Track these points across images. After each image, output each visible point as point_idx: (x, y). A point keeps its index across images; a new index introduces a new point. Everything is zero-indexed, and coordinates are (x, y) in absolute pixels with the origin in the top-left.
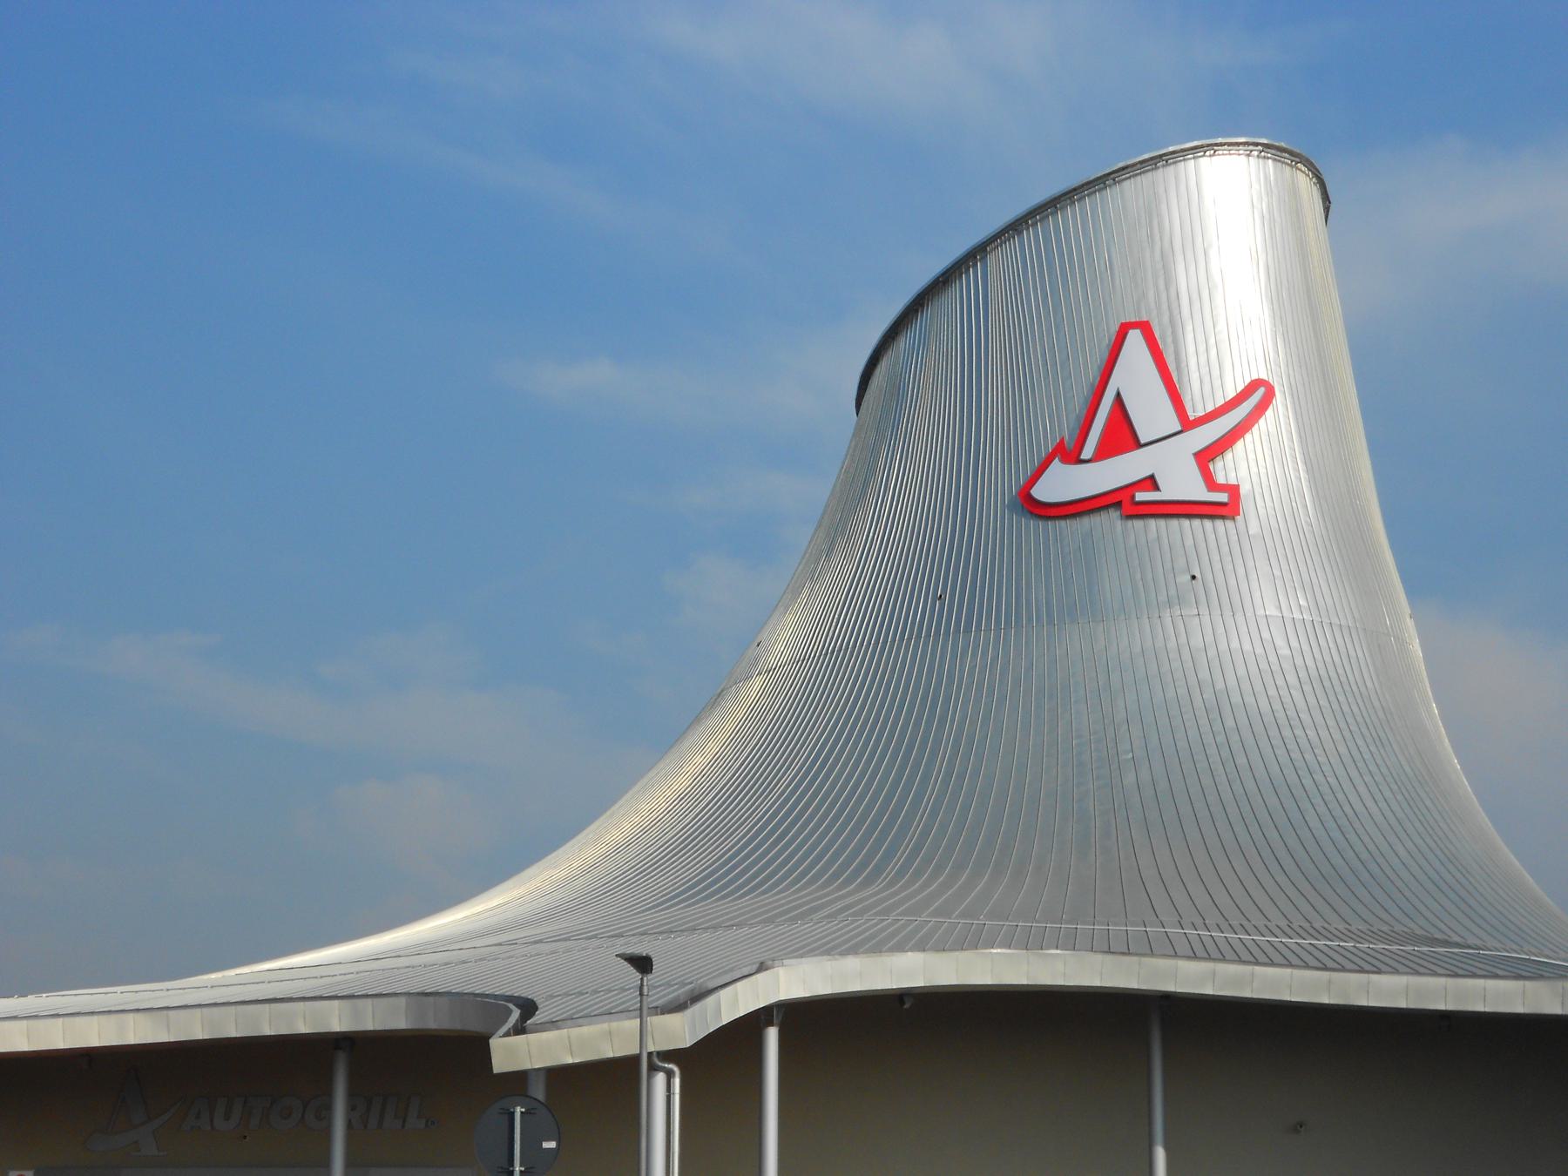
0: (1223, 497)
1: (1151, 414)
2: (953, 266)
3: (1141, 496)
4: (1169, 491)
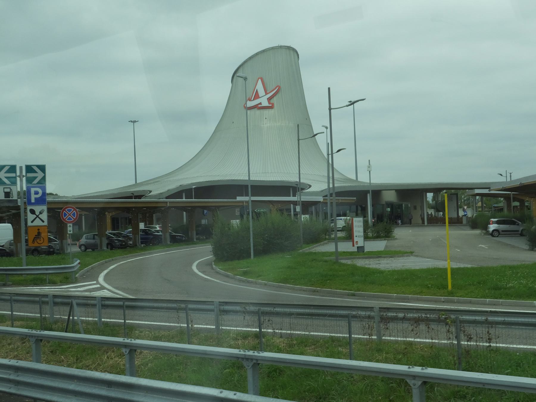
0: (271, 105)
1: (261, 92)
2: (254, 55)
3: (259, 106)
4: (263, 105)
